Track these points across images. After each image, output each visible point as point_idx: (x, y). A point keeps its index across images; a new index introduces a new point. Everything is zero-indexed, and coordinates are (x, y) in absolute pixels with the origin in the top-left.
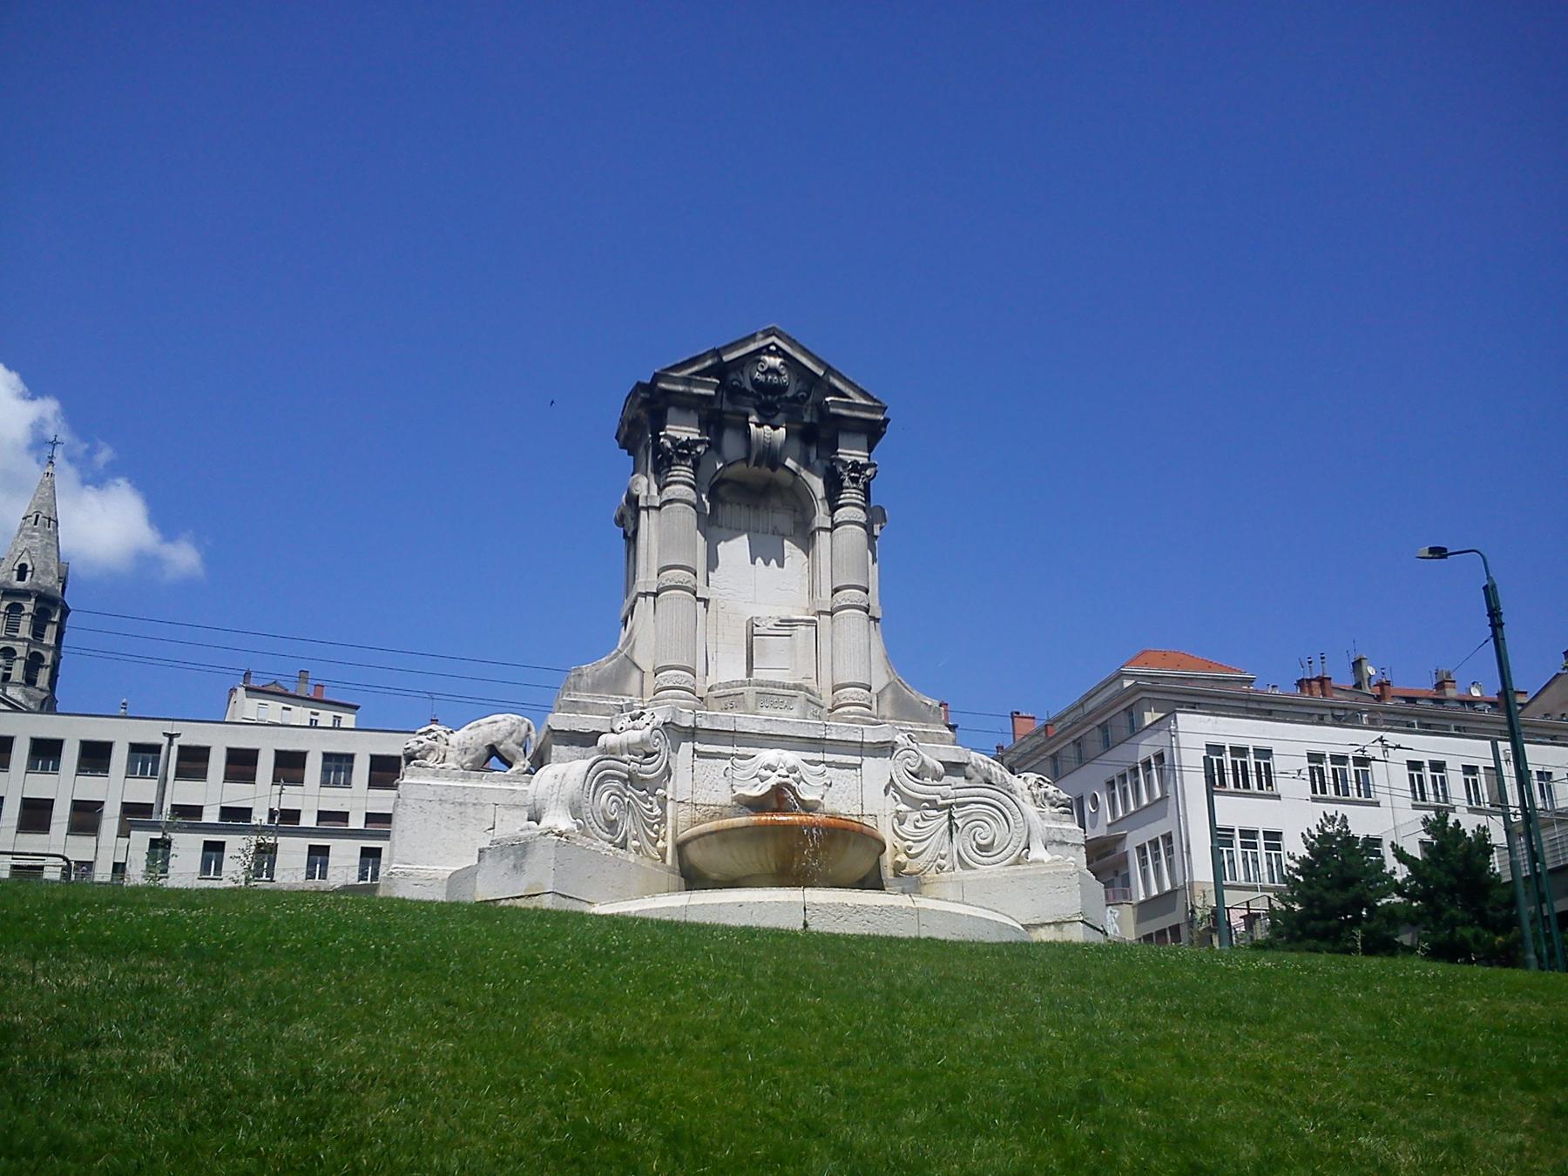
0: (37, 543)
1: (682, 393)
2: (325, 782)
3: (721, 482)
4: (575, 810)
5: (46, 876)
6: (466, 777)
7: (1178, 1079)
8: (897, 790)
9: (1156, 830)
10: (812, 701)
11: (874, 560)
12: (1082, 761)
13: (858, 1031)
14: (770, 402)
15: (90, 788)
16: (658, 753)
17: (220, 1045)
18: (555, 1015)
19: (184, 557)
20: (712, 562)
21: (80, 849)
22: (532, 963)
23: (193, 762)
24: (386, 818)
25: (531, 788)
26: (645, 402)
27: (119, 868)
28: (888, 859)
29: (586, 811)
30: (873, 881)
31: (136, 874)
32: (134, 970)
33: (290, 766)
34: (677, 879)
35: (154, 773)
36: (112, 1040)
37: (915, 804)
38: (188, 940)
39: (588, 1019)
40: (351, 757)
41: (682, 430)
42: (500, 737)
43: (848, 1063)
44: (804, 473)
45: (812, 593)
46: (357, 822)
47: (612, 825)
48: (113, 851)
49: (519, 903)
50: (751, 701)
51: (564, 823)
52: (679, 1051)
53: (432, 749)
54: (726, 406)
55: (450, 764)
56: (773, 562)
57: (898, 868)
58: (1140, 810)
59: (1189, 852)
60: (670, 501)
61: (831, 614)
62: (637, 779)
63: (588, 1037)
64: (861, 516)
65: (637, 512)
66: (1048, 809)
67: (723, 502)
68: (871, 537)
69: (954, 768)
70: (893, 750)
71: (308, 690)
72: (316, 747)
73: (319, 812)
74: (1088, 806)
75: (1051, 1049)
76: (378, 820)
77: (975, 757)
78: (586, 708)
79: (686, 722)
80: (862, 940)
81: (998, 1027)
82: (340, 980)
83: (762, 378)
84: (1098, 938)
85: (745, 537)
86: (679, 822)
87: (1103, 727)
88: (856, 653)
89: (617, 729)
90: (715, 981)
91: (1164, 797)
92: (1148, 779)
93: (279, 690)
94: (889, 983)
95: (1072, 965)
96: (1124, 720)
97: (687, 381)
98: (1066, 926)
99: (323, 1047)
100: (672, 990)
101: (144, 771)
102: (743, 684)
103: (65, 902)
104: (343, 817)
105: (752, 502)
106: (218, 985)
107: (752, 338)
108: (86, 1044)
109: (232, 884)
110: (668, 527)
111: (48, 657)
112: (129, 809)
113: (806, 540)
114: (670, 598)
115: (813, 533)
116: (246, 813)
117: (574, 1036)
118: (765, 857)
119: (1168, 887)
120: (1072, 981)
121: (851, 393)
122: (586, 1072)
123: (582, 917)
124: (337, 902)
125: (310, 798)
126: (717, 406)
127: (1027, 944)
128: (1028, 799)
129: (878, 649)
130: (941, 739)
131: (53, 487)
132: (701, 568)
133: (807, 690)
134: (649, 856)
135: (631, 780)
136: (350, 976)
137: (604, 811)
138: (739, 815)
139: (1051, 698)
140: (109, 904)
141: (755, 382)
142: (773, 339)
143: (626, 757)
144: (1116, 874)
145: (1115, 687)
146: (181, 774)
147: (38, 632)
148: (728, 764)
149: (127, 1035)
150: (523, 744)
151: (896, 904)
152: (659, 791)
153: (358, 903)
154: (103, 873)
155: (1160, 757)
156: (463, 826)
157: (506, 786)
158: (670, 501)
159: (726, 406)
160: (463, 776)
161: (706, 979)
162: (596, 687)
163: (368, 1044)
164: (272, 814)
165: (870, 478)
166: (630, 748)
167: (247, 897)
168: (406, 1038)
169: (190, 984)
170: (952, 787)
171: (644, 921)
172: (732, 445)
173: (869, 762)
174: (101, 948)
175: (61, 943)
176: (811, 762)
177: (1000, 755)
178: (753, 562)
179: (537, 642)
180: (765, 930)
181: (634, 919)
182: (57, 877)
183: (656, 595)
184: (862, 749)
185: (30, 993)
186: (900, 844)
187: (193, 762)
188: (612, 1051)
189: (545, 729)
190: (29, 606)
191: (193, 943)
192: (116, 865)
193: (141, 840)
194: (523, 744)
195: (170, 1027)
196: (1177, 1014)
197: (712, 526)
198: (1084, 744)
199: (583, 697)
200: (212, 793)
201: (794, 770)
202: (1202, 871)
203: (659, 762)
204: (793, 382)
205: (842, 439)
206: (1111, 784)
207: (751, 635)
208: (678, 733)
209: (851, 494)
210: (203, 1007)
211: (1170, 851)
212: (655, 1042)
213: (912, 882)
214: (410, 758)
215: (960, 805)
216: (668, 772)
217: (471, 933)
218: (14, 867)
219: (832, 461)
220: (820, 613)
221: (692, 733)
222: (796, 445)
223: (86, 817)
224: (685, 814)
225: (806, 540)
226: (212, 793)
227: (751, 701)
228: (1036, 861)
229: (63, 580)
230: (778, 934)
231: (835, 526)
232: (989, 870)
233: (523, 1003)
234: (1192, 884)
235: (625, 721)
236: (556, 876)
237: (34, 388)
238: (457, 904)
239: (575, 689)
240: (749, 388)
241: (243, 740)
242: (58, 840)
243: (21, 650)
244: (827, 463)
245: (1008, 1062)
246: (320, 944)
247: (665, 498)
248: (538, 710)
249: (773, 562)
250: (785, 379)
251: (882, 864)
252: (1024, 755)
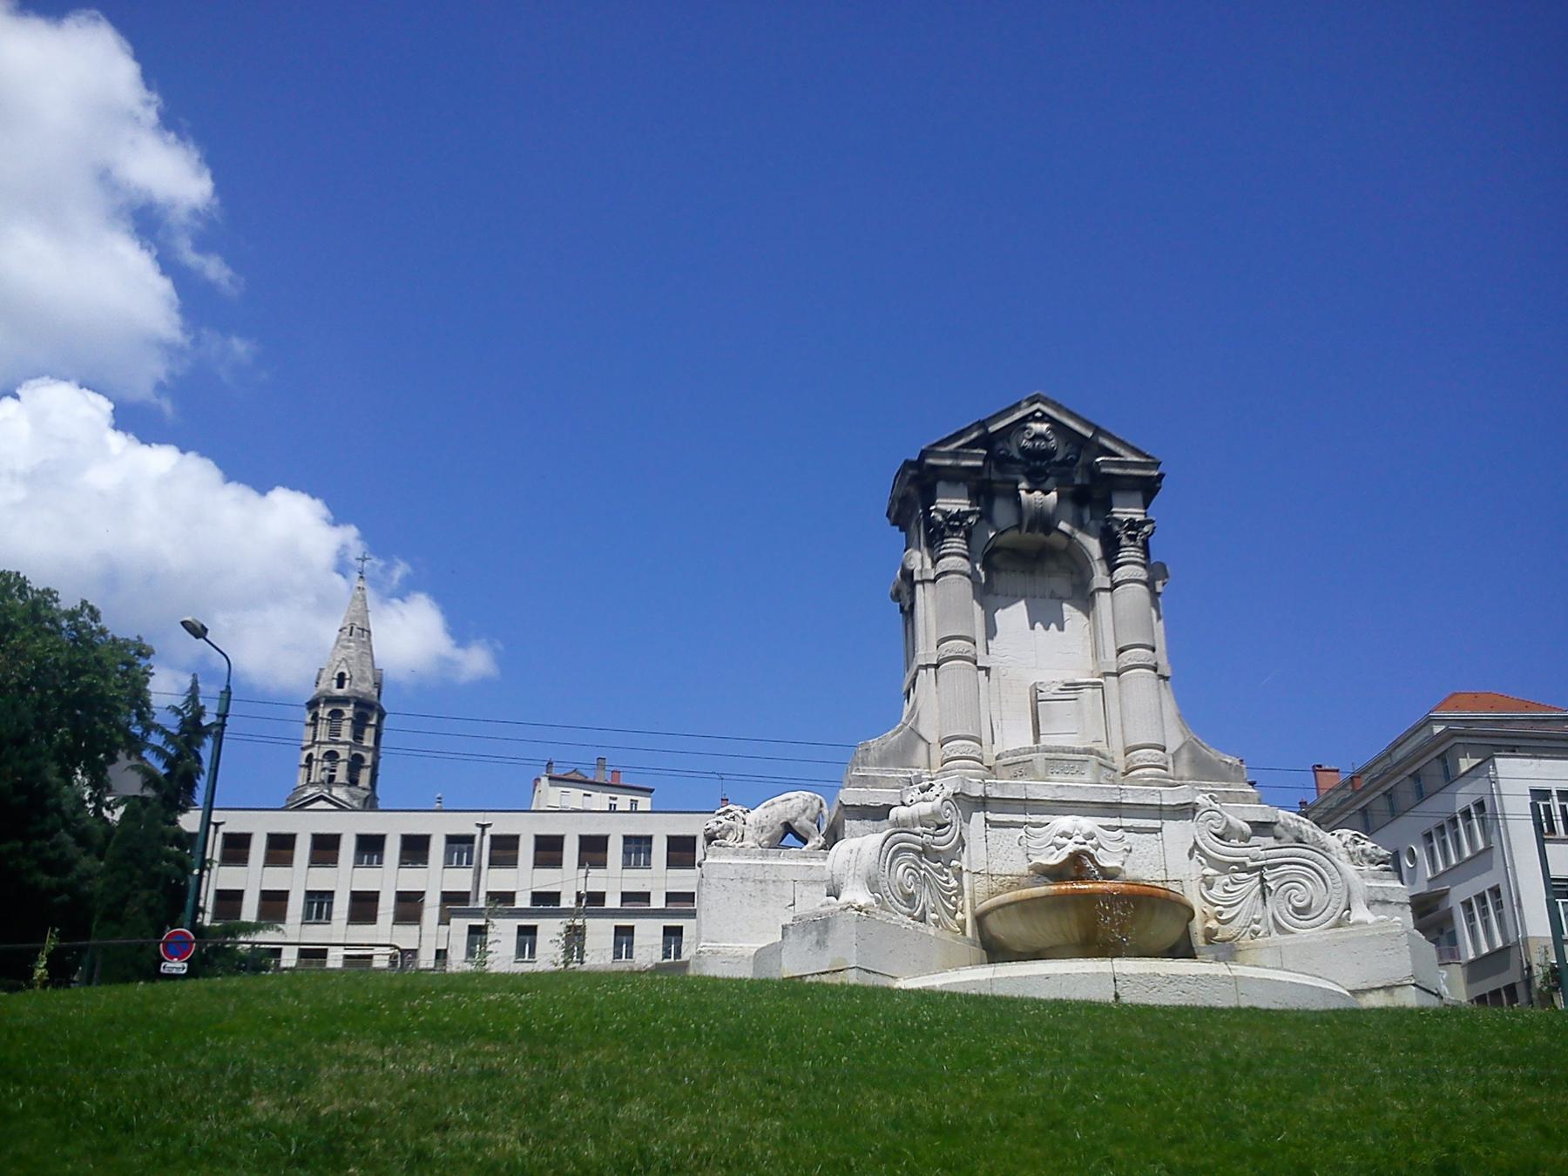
0: (353, 652)
1: (950, 467)
2: (626, 865)
3: (995, 550)
4: (873, 885)
5: (330, 964)
6: (764, 855)
7: (1544, 1153)
8: (1203, 853)
9: (1482, 883)
10: (1105, 765)
11: (1159, 618)
12: (1395, 814)
13: (1188, 1107)
14: (1039, 467)
15: (412, 879)
16: (951, 824)
17: (560, 1126)
18: (875, 1092)
19: (477, 661)
20: (991, 631)
21: (406, 937)
22: (847, 1040)
23: (504, 851)
24: (689, 897)
25: (828, 864)
26: (914, 479)
27: (441, 955)
28: (1197, 926)
29: (883, 885)
30: (1182, 949)
31: (458, 962)
32: (473, 1054)
33: (593, 850)
34: (978, 952)
35: (469, 862)
36: (460, 1124)
37: (1223, 867)
38: (521, 1024)
39: (909, 1096)
40: (649, 839)
41: (952, 503)
42: (794, 814)
43: (1182, 1140)
44: (1079, 535)
45: (1095, 655)
46: (658, 902)
47: (909, 898)
48: (433, 937)
49: (824, 978)
50: (1040, 767)
51: (863, 897)
52: (1005, 1129)
53: (731, 829)
54: (995, 476)
55: (749, 843)
56: (1053, 626)
57: (1210, 935)
58: (1463, 862)
59: (1520, 906)
60: (945, 573)
61: (1118, 675)
62: (931, 851)
63: (910, 1114)
64: (1141, 573)
65: (913, 585)
66: (1366, 867)
67: (997, 570)
68: (1154, 595)
69: (1261, 828)
70: (1195, 811)
71: (605, 777)
72: (616, 830)
74: (1406, 863)
75: (1399, 1122)
76: (681, 901)
77: (1283, 815)
78: (875, 782)
79: (977, 791)
80: (1180, 1011)
81: (1339, 1100)
82: (665, 1059)
83: (1029, 444)
84: (1432, 1002)
85: (1022, 603)
86: (976, 894)
87: (1415, 777)
88: (1147, 713)
89: (907, 801)
90: (1033, 1056)
91: (1488, 849)
92: (1469, 830)
93: (579, 777)
94: (1214, 1055)
95: (1410, 1032)
96: (1437, 768)
97: (955, 454)
98: (1397, 991)
99: (657, 1127)
100: (989, 1066)
101: (460, 861)
102: (1031, 751)
103: (403, 991)
104: (645, 897)
105: (1026, 567)
106: (552, 1068)
107: (1017, 406)
108: (437, 1128)
109: (553, 968)
110: (946, 601)
111: (368, 758)
112: (448, 898)
113: (1086, 602)
114: (948, 668)
115: (1092, 594)
116: (554, 897)
117: (898, 1114)
118: (1068, 925)
119: (1499, 944)
120: (1412, 1048)
121: (1122, 452)
122: (914, 1149)
123: (890, 993)
124: (653, 982)
125: (613, 880)
126: (985, 476)
127: (1357, 1011)
128: (1345, 857)
129: (1170, 708)
130: (1245, 798)
131: (364, 600)
132: (980, 637)
133: (1098, 754)
134: (948, 928)
135: (925, 852)
136: (675, 1056)
137: (901, 884)
138: (1037, 885)
139: (1355, 750)
140: (445, 991)
141: (1022, 450)
142: (1038, 406)
143: (918, 829)
144: (1441, 931)
145: (1424, 734)
146: (493, 863)
147: (358, 735)
148: (1022, 832)
149: (473, 1118)
150: (816, 820)
151: (1212, 973)
152: (954, 863)
153: (674, 983)
154: (426, 960)
155: (1480, 806)
156: (764, 903)
157: (803, 863)
158: (945, 573)
159: (995, 476)
160: (762, 854)
161: (1023, 1054)
162: (883, 761)
163: (698, 1123)
164: (579, 896)
165: (1148, 535)
166: (921, 820)
167: (570, 979)
168: (733, 1118)
169: (526, 1068)
170: (1261, 848)
171: (952, 995)
172: (1003, 513)
173: (1170, 826)
174: (440, 1033)
175: (405, 1030)
176: (1108, 828)
177: (1305, 810)
178: (1032, 628)
179: (825, 720)
180: (1077, 1002)
181: (942, 994)
182: (386, 964)
183: (937, 666)
184: (1161, 812)
185: (382, 1079)
186: (1210, 910)
187: (504, 851)
188: (938, 1130)
189: (837, 804)
190: (349, 711)
191: (526, 1027)
192: (438, 951)
193: (460, 926)
194: (816, 820)
195: (513, 1110)
196: (1534, 1081)
197: (989, 595)
198: (1398, 793)
199: (872, 771)
200: (524, 879)
201: (1091, 836)
202: (1537, 924)
203: (951, 834)
204: (1061, 448)
205: (1116, 498)
206: (1428, 837)
207: (1035, 702)
208: (969, 804)
209: (1129, 553)
210: (541, 1089)
211: (1499, 905)
212: (980, 1120)
213: (1227, 950)
214: (710, 838)
215: (1271, 867)
216: (962, 843)
217: (784, 1010)
218: (347, 957)
219: (1108, 520)
220: (1106, 674)
221: (983, 803)
222: (1069, 508)
223: (409, 906)
224: (982, 885)
225: (1086, 602)
226: (524, 879)
227: (1040, 767)
228: (1359, 923)
229: (378, 685)
230: (1091, 1006)
231: (1115, 585)
232: (1307, 933)
233: (843, 1080)
234: (1526, 939)
235: (915, 794)
236: (859, 951)
237: (337, 518)
238: (767, 981)
239: (864, 764)
240: (1018, 456)
241: (550, 827)
242: (384, 931)
243: (344, 752)
244: (1101, 523)
245: (1354, 1137)
246: (643, 1025)
247: (939, 570)
248: (827, 785)
249: (1053, 626)
250: (1053, 443)
251: (1193, 931)
252: (1329, 811)
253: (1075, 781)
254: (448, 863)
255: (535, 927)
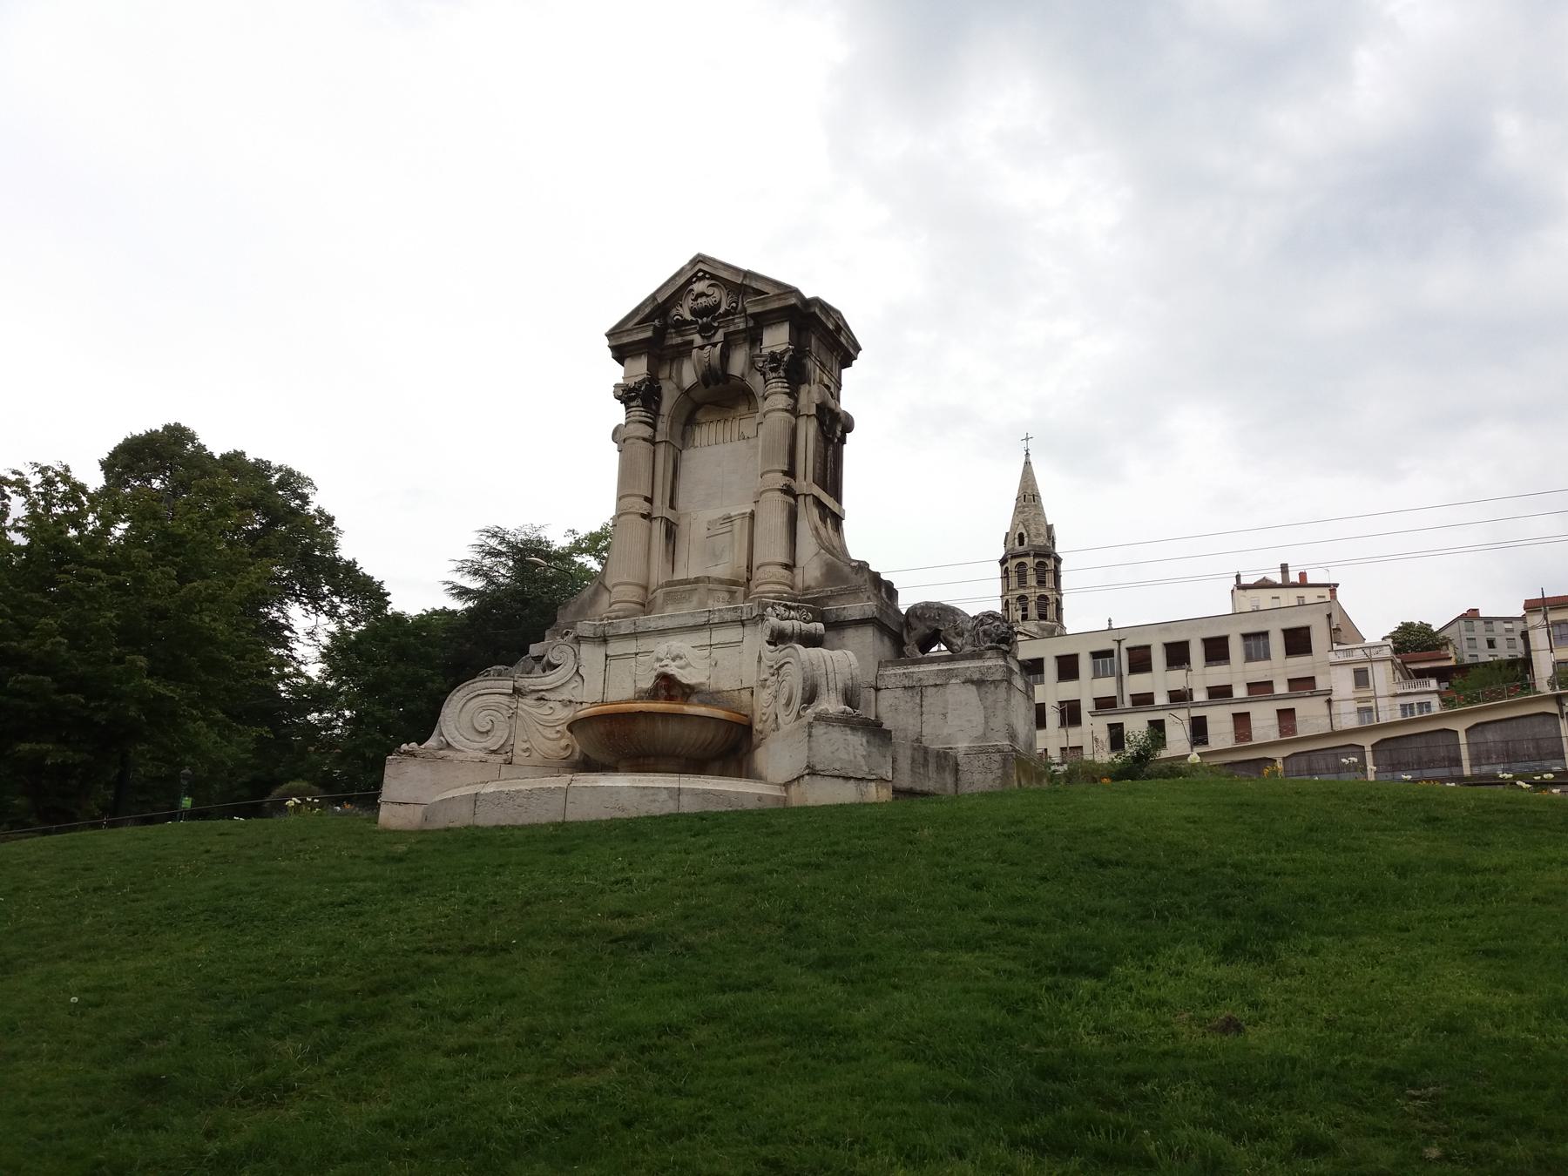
40: (1265, 634)
73: (1290, 681)
104: (1268, 686)
146: (1132, 671)
223: (1071, 714)
253: (686, 608)
254: (1096, 675)
255: (1248, 714)
